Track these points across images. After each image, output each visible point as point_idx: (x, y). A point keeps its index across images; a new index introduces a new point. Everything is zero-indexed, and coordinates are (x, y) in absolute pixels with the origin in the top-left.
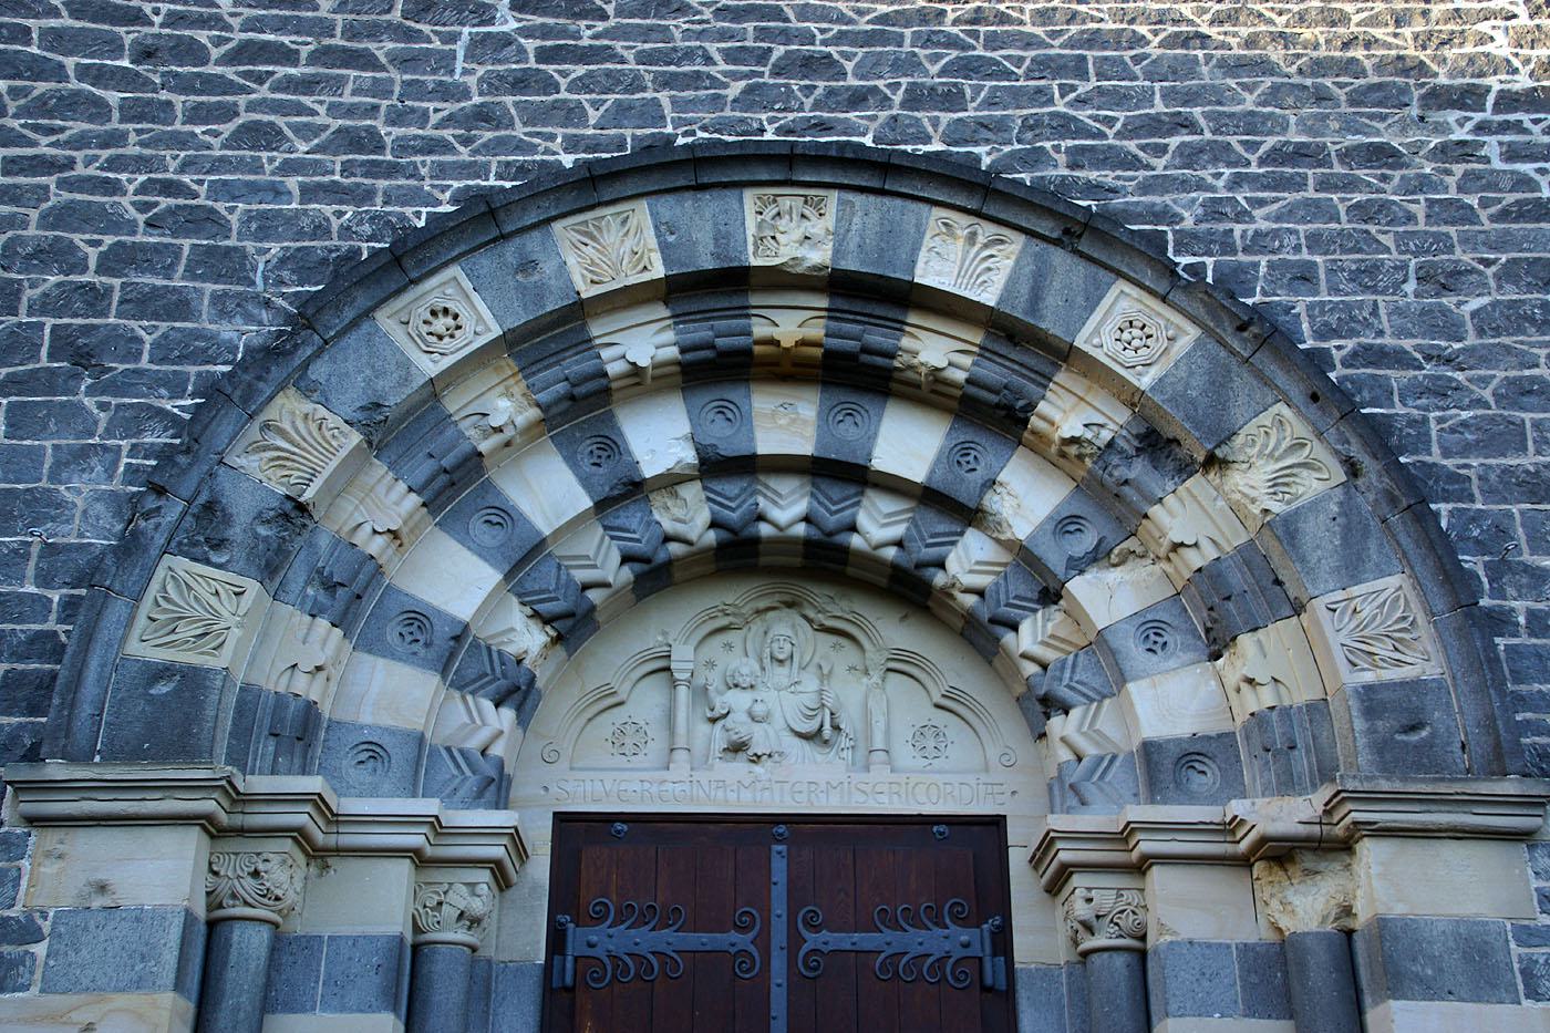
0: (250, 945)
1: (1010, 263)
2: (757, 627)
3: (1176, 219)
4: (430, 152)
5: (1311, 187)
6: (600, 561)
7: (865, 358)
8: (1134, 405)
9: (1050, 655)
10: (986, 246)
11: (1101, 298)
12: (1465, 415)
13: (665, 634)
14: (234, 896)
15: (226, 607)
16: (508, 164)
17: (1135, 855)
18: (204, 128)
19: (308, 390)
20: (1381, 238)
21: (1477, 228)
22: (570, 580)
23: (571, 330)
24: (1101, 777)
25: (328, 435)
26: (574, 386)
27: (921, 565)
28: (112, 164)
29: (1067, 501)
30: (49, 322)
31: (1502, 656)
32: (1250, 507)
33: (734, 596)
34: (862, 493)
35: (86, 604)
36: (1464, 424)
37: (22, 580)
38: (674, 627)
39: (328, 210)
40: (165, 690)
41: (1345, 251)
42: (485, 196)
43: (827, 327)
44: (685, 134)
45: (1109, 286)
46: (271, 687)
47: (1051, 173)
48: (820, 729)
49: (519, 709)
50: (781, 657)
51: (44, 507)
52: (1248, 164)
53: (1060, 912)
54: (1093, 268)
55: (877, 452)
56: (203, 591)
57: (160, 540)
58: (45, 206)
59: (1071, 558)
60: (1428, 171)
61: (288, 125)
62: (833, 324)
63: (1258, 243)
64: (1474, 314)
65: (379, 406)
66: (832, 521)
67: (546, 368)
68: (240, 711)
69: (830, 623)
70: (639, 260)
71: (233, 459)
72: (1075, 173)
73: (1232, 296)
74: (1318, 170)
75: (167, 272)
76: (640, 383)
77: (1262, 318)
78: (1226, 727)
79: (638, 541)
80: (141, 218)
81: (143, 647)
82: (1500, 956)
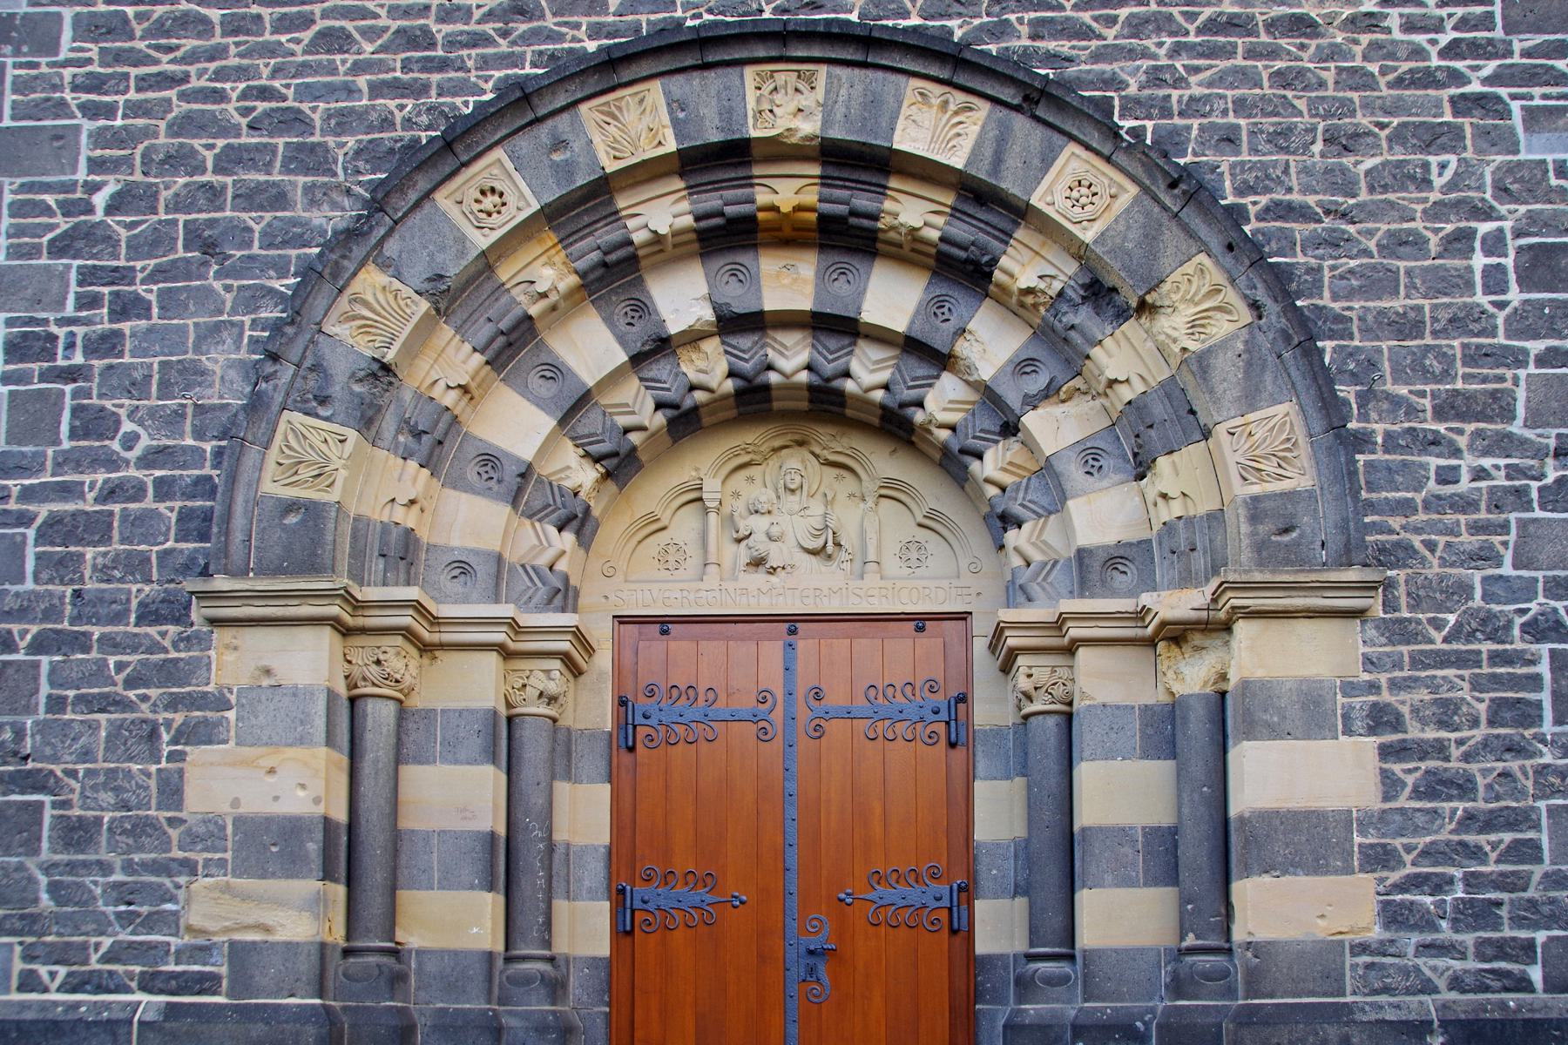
0: (380, 715)
1: (977, 128)
2: (773, 463)
3: (1120, 85)
4: (475, 46)
5: (1239, 56)
6: (636, 407)
7: (853, 221)
8: (1081, 258)
9: (1007, 479)
10: (956, 113)
11: (1054, 160)
12: (1353, 263)
13: (697, 469)
14: (364, 679)
15: (333, 451)
16: (541, 53)
17: (1066, 640)
18: (289, 36)
19: (384, 265)
20: (1296, 102)
21: (1376, 94)
22: (614, 425)
23: (601, 204)
24: (1045, 579)
25: (402, 303)
26: (605, 254)
27: (903, 405)
28: (220, 75)
29: (1025, 346)
30: (182, 218)
31: (1361, 470)
32: (1172, 346)
33: (752, 437)
34: (855, 344)
35: (228, 452)
36: (1351, 271)
37: (182, 436)
38: (703, 464)
39: (392, 104)
40: (295, 520)
41: (1265, 114)
42: (520, 83)
43: (820, 194)
44: (694, 17)
45: (1062, 148)
46: (376, 517)
47: (1015, 44)
48: (825, 546)
49: (578, 533)
50: (793, 487)
51: (194, 374)
52: (1187, 33)
53: (1010, 687)
54: (1049, 132)
55: (866, 306)
56: (316, 440)
57: (279, 398)
58: (170, 116)
59: (1026, 395)
60: (1339, 40)
61: (356, 28)
62: (827, 191)
63: (1192, 107)
64: (1368, 173)
65: (441, 277)
66: (829, 369)
67: (582, 239)
68: (355, 531)
69: (833, 458)
70: (655, 136)
71: (327, 328)
72: (1037, 44)
73: (1166, 155)
74: (1247, 40)
75: (268, 168)
76: (665, 251)
77: (1190, 175)
78: (1145, 535)
79: (668, 390)
80: (244, 122)
81: (273, 486)
82: (1329, 705)
